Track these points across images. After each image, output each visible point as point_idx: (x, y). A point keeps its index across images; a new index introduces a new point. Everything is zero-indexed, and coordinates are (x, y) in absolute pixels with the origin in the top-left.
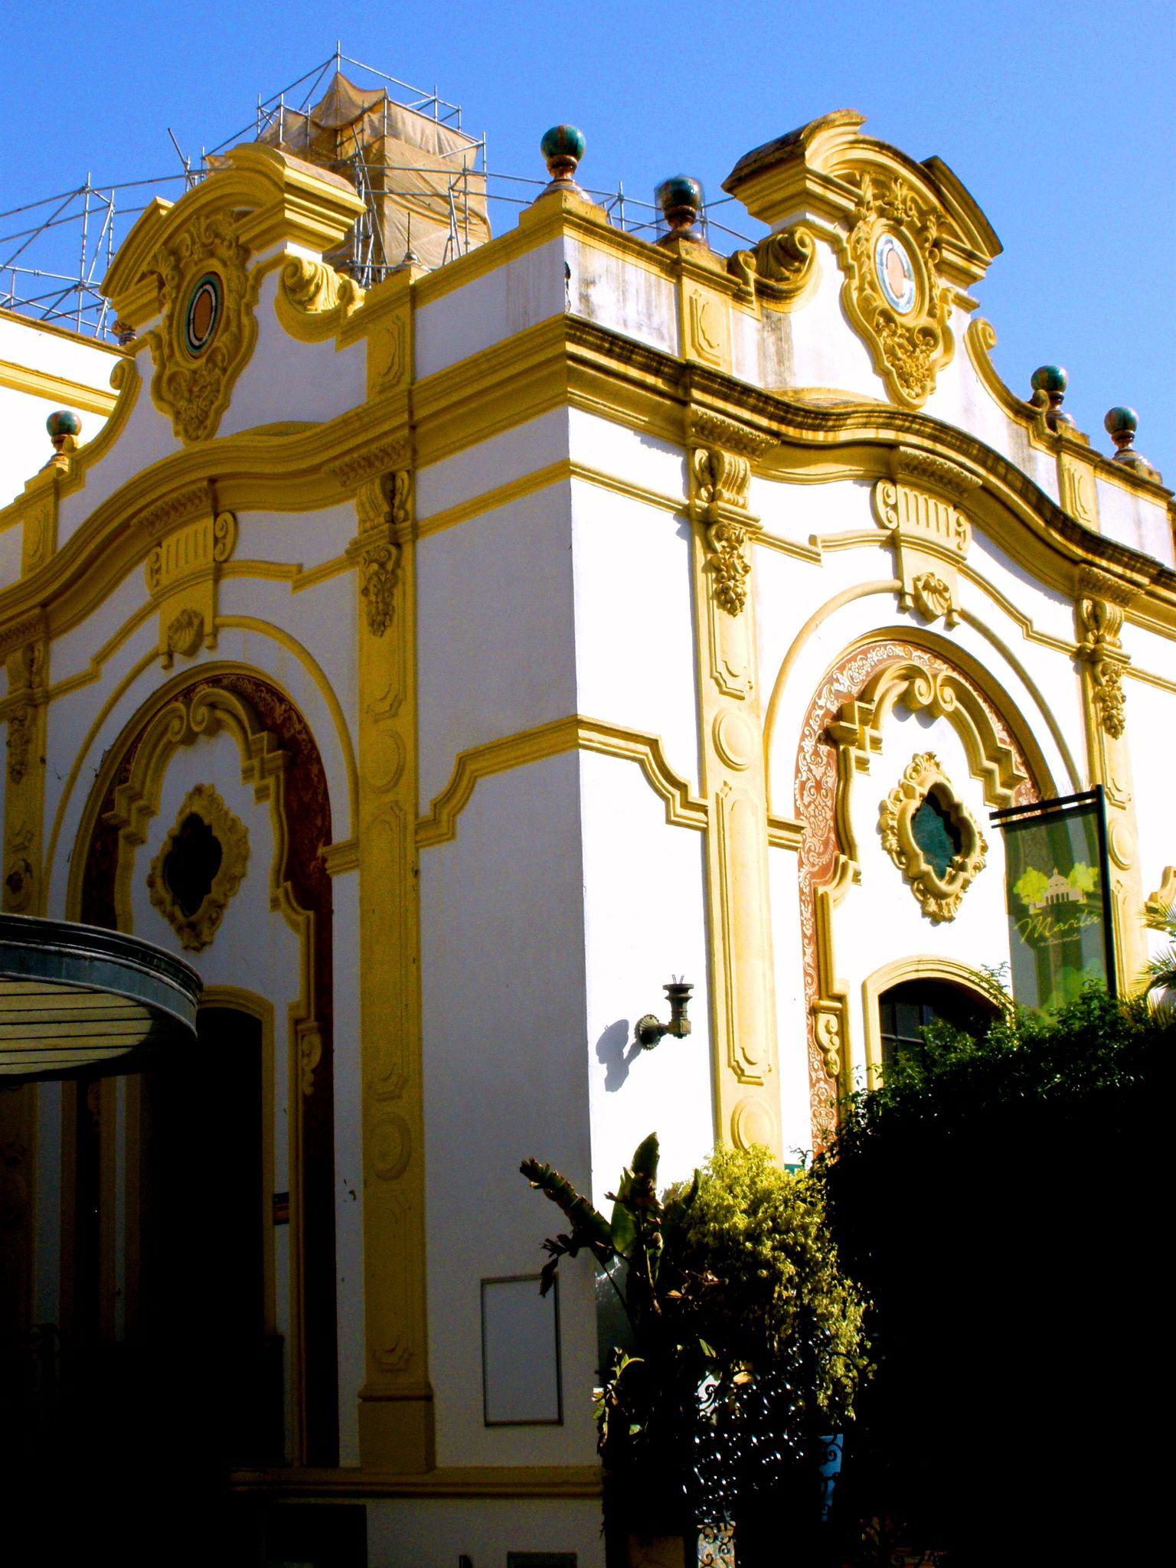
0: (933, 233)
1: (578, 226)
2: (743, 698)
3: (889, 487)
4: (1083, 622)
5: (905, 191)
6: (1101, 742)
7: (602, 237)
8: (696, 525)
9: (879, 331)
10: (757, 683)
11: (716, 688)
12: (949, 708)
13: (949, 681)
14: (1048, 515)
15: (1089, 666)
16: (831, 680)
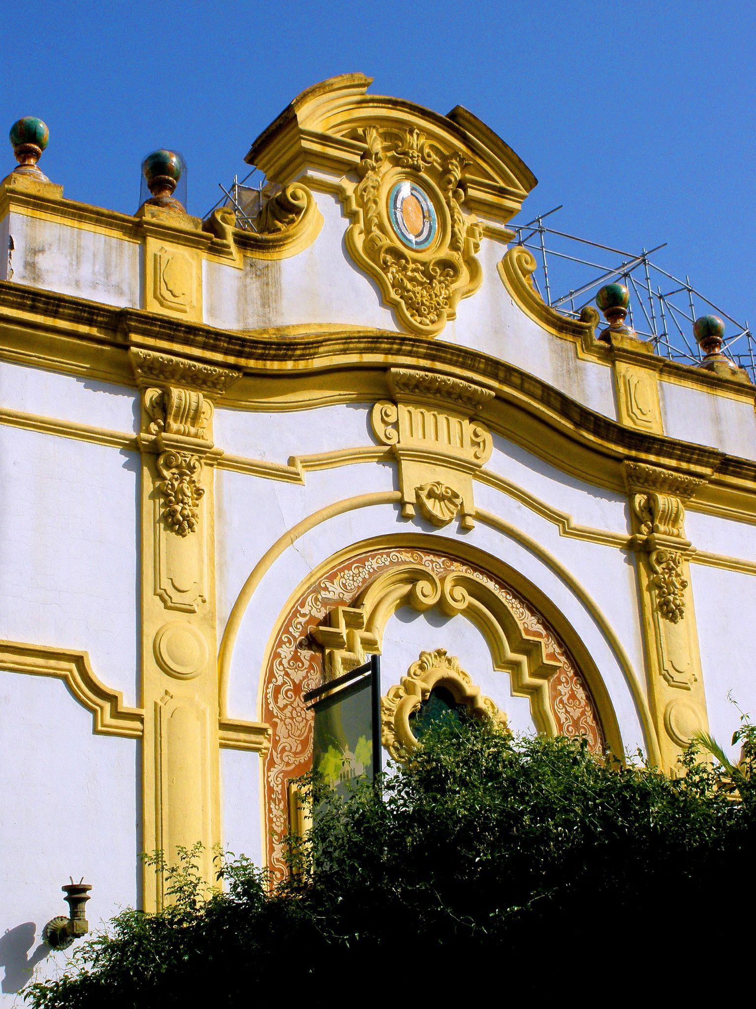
0: (457, 174)
1: (26, 203)
2: (193, 612)
3: (390, 408)
4: (636, 515)
5: (422, 140)
6: (657, 627)
7: (54, 211)
8: (145, 457)
9: (385, 267)
10: (213, 595)
11: (162, 605)
12: (462, 606)
13: (461, 581)
14: (577, 418)
15: (642, 555)
16: (316, 589)
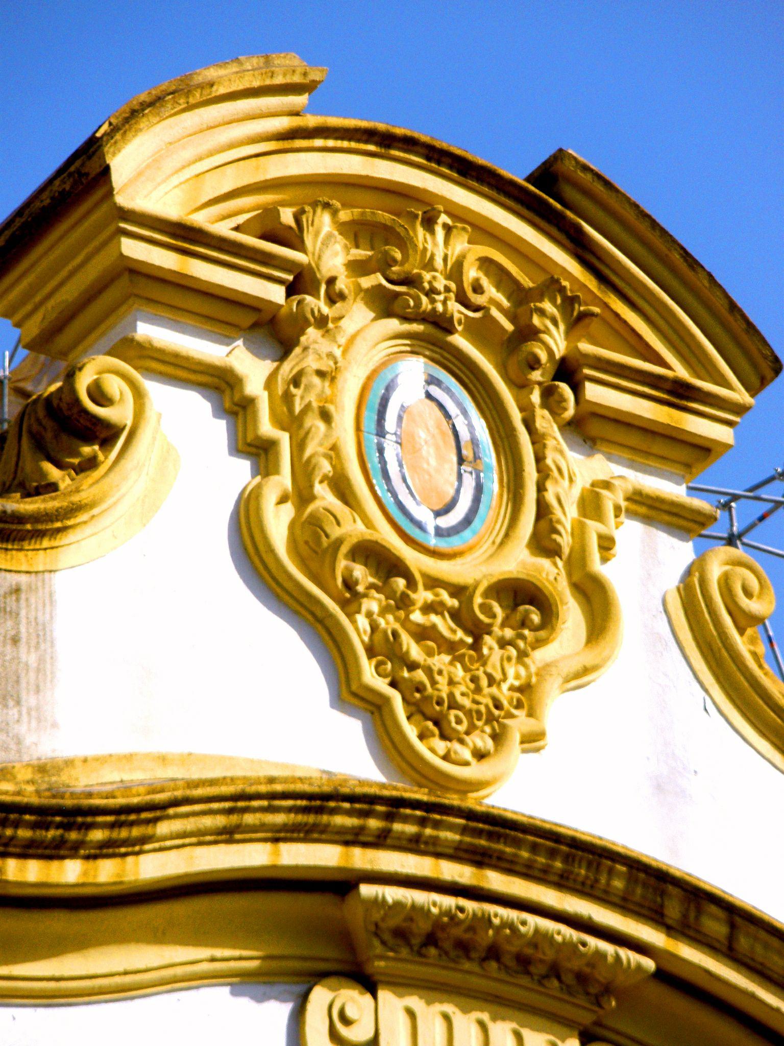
3: (355, 1001)
5: (460, 244)
9: (350, 596)
